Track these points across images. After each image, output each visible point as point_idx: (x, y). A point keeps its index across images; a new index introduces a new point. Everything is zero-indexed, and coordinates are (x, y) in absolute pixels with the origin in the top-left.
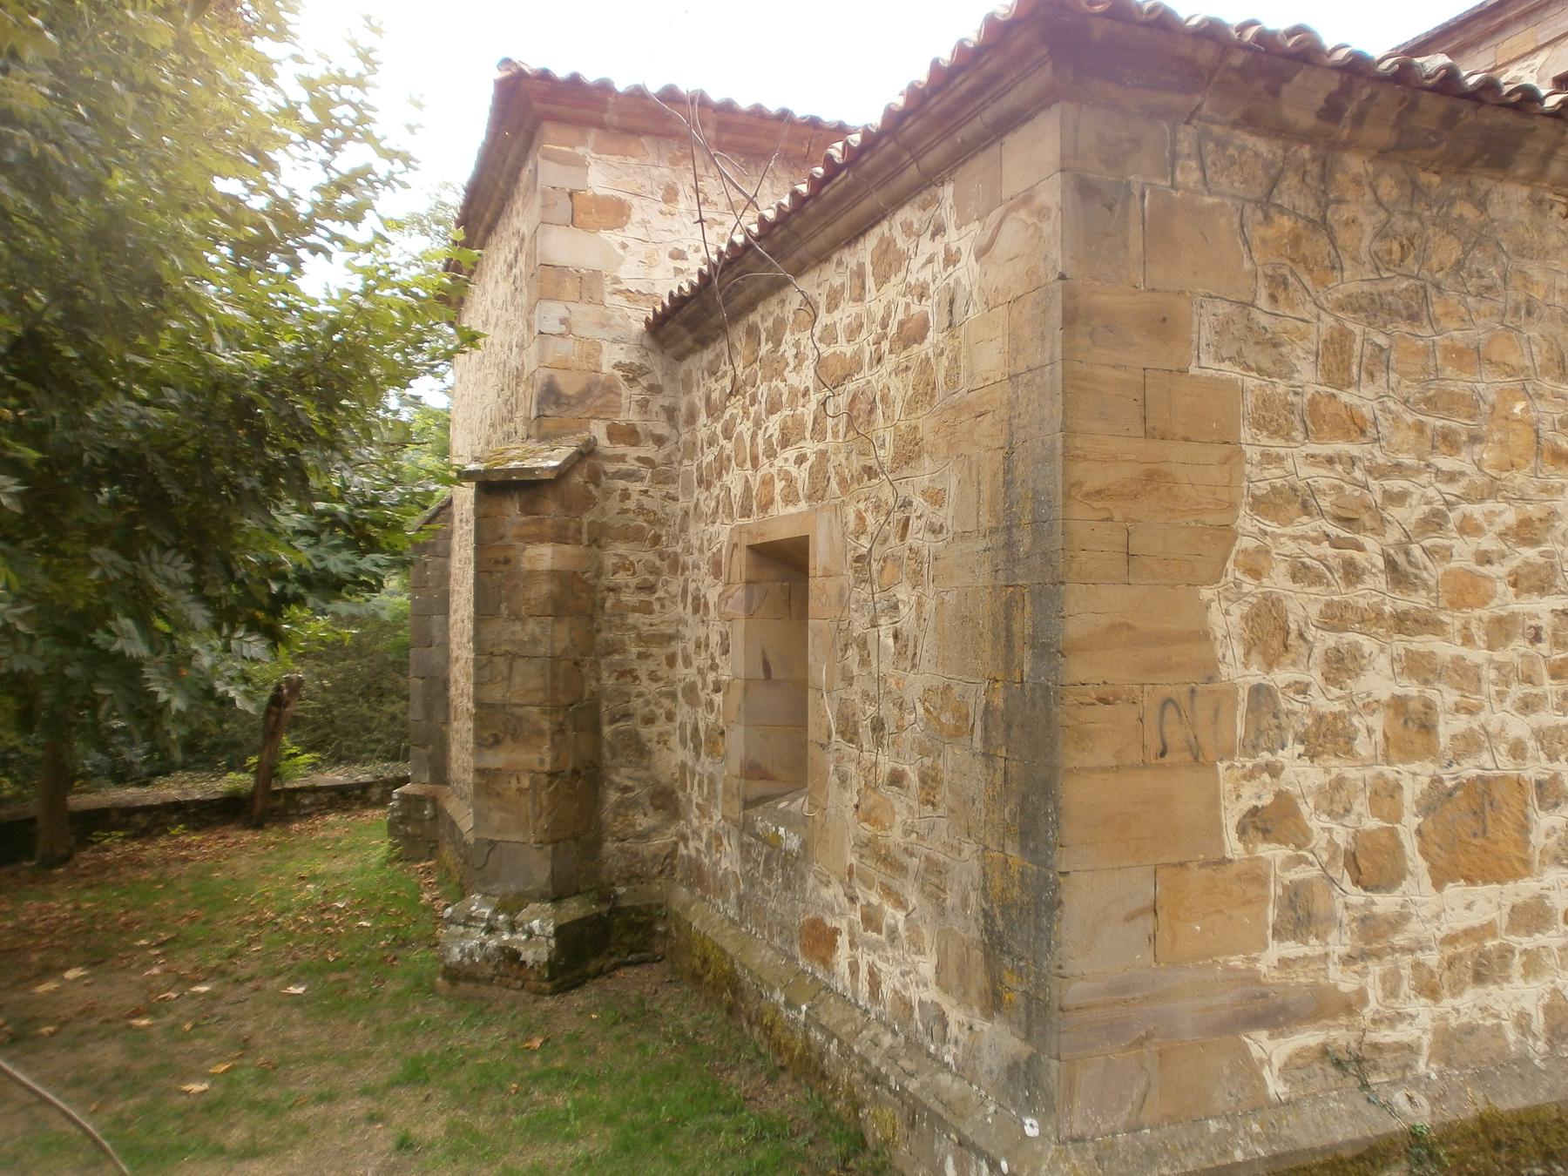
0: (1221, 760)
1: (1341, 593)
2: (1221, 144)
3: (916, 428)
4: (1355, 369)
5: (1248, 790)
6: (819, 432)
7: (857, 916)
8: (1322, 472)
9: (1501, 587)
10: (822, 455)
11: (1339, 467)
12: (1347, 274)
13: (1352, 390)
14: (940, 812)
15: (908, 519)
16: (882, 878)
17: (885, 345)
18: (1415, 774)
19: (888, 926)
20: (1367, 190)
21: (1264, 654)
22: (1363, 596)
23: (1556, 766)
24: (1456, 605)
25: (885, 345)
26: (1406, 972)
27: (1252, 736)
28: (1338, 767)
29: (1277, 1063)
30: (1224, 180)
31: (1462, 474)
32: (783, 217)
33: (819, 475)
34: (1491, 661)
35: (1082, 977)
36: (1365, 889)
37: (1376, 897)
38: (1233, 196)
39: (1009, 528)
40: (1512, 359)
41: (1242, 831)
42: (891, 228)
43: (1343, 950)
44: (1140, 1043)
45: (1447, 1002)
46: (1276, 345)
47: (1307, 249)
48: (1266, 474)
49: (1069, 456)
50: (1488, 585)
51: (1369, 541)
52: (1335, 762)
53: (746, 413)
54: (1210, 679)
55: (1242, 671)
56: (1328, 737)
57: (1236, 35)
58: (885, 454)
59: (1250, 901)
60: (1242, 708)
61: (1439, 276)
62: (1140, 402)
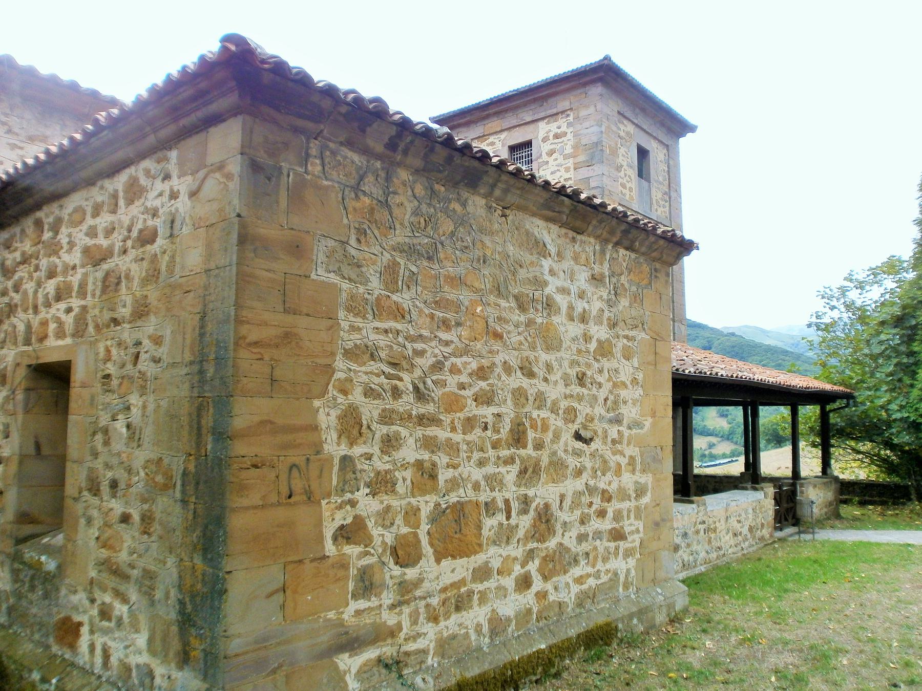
0: (323, 499)
1: (390, 404)
2: (334, 153)
3: (146, 296)
4: (400, 283)
5: (339, 515)
6: (82, 294)
7: (95, 612)
8: (382, 337)
9: (469, 401)
10: (84, 309)
11: (391, 335)
12: (397, 232)
13: (398, 294)
14: (153, 539)
15: (139, 353)
16: (112, 585)
17: (129, 243)
18: (427, 502)
19: (117, 617)
20: (409, 189)
21: (349, 438)
22: (402, 406)
23: (494, 494)
24: (448, 411)
25: (129, 243)
26: (422, 610)
27: (341, 485)
28: (388, 500)
29: (354, 671)
30: (334, 173)
31: (452, 342)
32: (64, 153)
33: (81, 321)
34: (464, 440)
35: (239, 636)
36: (401, 567)
37: (407, 571)
38: (338, 182)
39: (201, 362)
40: (476, 284)
41: (335, 539)
42: (137, 171)
43: (390, 602)
44: (274, 671)
45: (442, 624)
46: (359, 266)
47: (377, 216)
48: (352, 337)
49: (239, 321)
50: (464, 401)
51: (406, 377)
52: (386, 497)
53: (31, 278)
54: (318, 453)
55: (336, 447)
56: (382, 484)
57: (343, 97)
58: (125, 312)
59: (339, 579)
60: (336, 469)
61: (443, 238)
62: (282, 292)
